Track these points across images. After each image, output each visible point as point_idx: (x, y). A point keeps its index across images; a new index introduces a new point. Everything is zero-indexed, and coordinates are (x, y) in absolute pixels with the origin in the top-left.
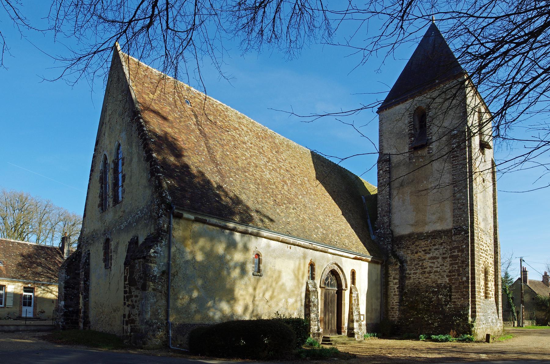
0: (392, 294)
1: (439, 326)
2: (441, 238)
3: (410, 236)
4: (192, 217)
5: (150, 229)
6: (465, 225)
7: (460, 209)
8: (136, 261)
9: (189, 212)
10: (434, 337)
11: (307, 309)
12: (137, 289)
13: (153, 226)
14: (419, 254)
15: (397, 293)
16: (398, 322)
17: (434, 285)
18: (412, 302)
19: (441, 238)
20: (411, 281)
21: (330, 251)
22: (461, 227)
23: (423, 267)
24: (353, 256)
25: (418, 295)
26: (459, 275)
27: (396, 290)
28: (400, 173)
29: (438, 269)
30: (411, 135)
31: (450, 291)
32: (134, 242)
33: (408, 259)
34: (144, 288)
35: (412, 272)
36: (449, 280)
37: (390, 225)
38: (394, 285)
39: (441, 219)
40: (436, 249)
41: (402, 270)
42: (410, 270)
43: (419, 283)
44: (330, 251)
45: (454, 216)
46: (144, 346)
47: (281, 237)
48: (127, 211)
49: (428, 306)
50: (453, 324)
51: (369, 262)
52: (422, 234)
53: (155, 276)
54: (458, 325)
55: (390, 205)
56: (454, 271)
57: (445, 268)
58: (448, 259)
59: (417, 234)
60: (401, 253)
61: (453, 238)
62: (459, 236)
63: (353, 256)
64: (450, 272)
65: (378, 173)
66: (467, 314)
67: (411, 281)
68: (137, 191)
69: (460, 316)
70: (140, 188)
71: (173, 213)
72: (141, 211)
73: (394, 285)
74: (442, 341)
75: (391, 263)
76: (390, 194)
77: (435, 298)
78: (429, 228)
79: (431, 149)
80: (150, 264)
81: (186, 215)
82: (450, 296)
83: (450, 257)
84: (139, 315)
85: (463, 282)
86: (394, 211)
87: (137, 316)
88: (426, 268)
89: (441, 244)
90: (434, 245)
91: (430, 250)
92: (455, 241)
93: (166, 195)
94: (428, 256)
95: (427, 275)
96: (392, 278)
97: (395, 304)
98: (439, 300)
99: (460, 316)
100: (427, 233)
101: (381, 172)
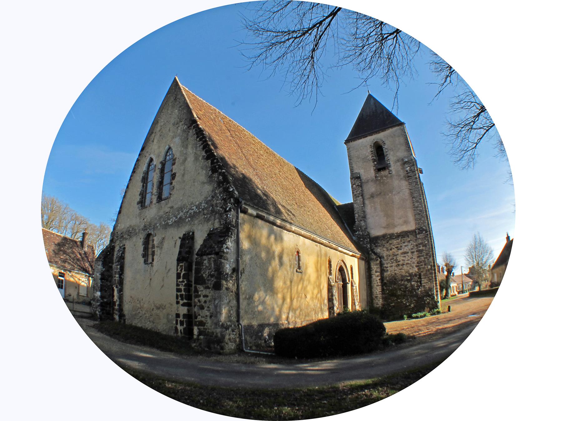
0: (375, 285)
1: (415, 306)
2: (408, 236)
3: (384, 236)
4: (254, 213)
5: (213, 224)
6: (424, 226)
7: (419, 214)
8: (204, 257)
9: (253, 208)
10: (414, 315)
11: (331, 303)
12: (207, 288)
13: (217, 220)
14: (393, 250)
15: (379, 284)
16: (382, 308)
17: (407, 275)
18: (391, 290)
19: (408, 236)
20: (389, 273)
21: (340, 249)
22: (421, 228)
23: (397, 261)
24: (351, 253)
25: (395, 284)
26: (425, 265)
27: (378, 281)
28: (370, 188)
29: (409, 262)
30: (374, 161)
31: (420, 278)
32: (188, 240)
33: (385, 255)
34: (217, 286)
35: (389, 265)
36: (418, 269)
37: (366, 228)
38: (376, 278)
39: (406, 222)
40: (406, 246)
41: (381, 264)
42: (387, 264)
43: (395, 274)
44: (340, 249)
45: (416, 220)
46: (222, 351)
47: (313, 236)
48: (175, 207)
49: (405, 291)
50: (425, 303)
51: (358, 259)
52: (393, 234)
53: (227, 274)
54: (429, 303)
55: (364, 212)
56: (421, 262)
57: (414, 260)
58: (416, 253)
59: (389, 234)
60: (378, 250)
61: (418, 236)
62: (422, 235)
63: (351, 253)
64: (418, 263)
65: (352, 187)
66: (434, 294)
67: (389, 273)
68: (193, 186)
69: (429, 296)
70: (196, 184)
71: (241, 208)
72: (198, 207)
73: (376, 278)
74: (421, 317)
75: (372, 259)
76: (364, 203)
77: (409, 285)
78: (398, 230)
79: (391, 171)
80: (223, 261)
81: (250, 211)
82: (420, 282)
83: (417, 251)
84: (211, 317)
85: (429, 270)
86: (368, 216)
87: (208, 318)
88: (399, 262)
89: (409, 242)
90: (404, 243)
91: (401, 247)
92: (419, 239)
93: (233, 190)
94: (400, 251)
95: (401, 267)
96: (374, 271)
97: (378, 293)
98: (412, 286)
99: (429, 296)
100: (397, 233)
101: (354, 186)
